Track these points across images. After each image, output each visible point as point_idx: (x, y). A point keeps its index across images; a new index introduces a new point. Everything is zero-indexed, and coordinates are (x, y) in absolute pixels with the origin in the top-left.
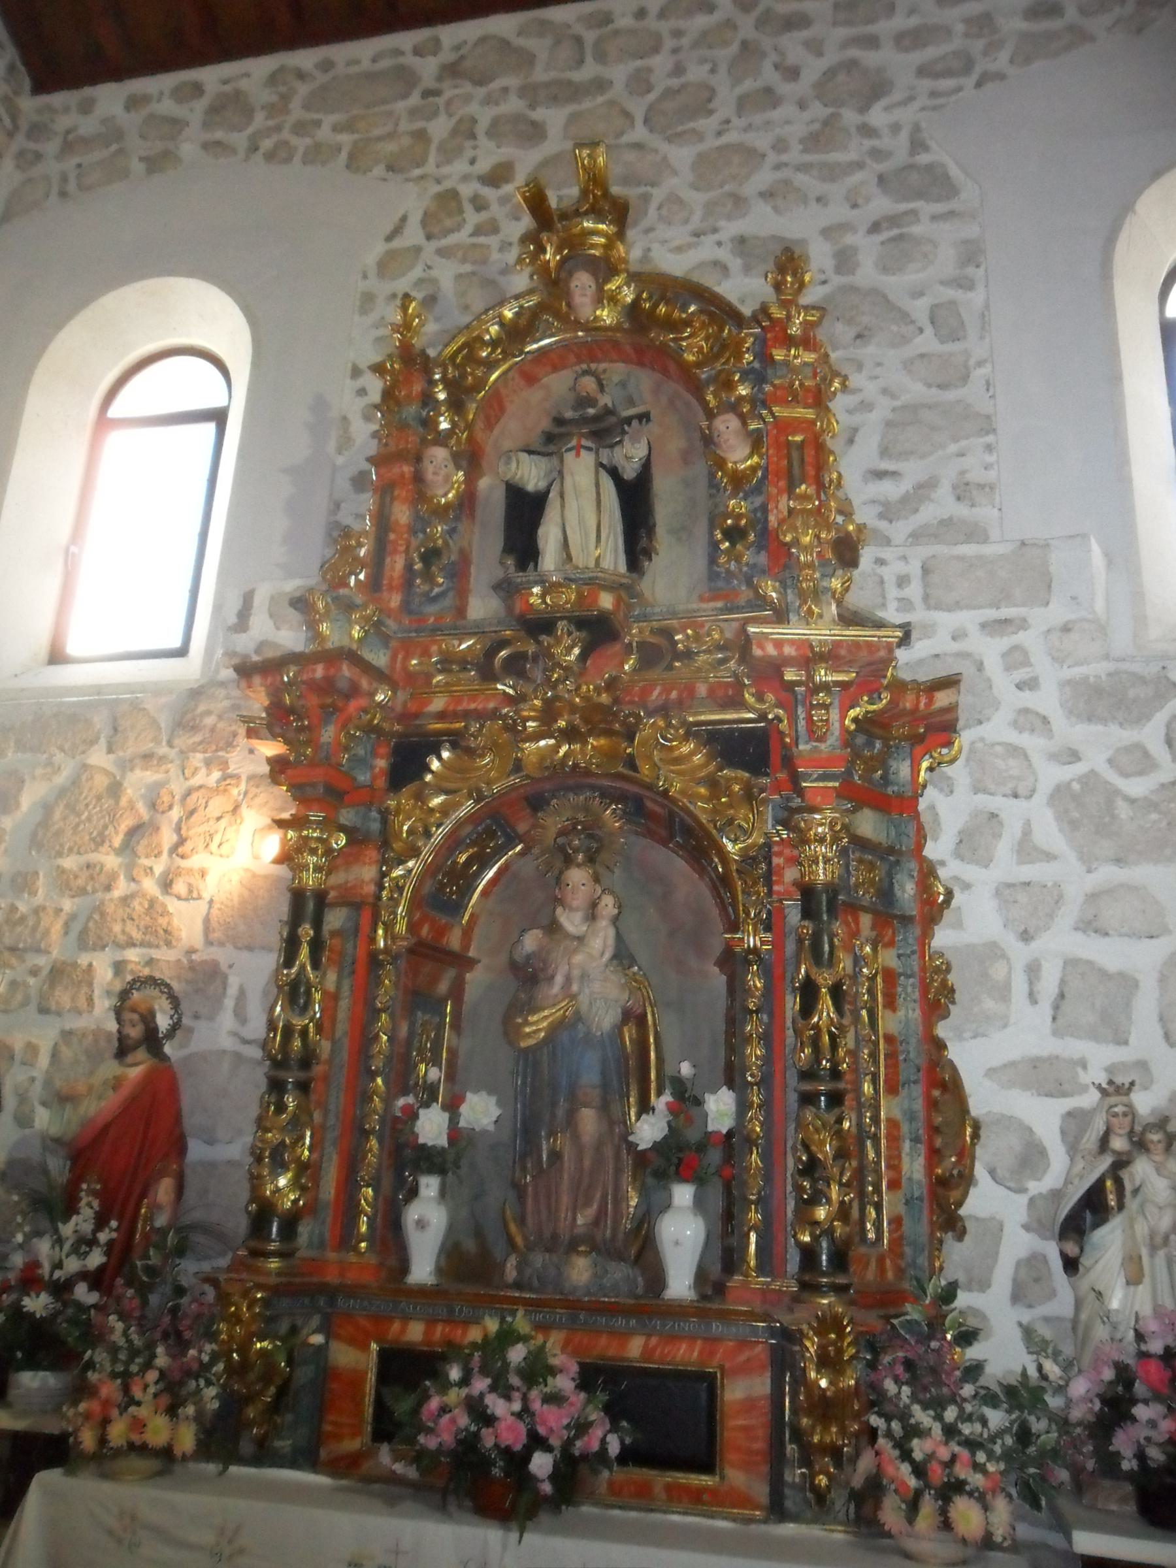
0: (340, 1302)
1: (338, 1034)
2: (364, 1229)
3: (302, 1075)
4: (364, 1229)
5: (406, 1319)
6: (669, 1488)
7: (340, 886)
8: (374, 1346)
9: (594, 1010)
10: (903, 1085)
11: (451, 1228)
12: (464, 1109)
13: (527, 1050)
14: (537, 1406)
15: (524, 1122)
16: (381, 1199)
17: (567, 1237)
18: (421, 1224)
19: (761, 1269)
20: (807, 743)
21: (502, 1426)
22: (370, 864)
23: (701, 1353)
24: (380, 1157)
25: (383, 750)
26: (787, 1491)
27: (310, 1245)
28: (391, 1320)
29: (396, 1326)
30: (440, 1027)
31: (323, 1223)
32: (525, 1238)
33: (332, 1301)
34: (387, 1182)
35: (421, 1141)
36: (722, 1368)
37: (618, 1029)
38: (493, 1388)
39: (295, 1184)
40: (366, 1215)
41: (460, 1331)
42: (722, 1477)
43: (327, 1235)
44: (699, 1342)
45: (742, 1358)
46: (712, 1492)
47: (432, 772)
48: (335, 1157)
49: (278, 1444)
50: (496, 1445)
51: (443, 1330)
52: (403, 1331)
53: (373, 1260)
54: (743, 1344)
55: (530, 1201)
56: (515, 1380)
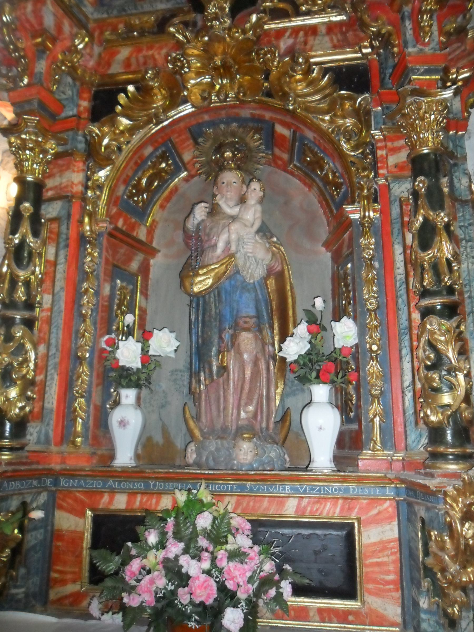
0: (63, 481)
1: (57, 288)
2: (79, 428)
3: (27, 314)
4: (79, 428)
5: (113, 492)
6: (320, 611)
7: (56, 187)
8: (89, 513)
9: (248, 264)
10: (469, 315)
11: (144, 427)
12: (152, 342)
13: (197, 296)
14: (223, 563)
15: (198, 348)
16: (92, 406)
17: (234, 427)
18: (123, 423)
19: (384, 446)
20: (414, 46)
21: (194, 584)
22: (78, 172)
23: (342, 509)
24: (91, 376)
25: (85, 95)
26: (423, 616)
27: (38, 442)
28: (102, 494)
29: (106, 498)
30: (133, 293)
31: (48, 425)
32: (201, 430)
33: (56, 483)
34: (96, 398)
35: (121, 364)
36: (359, 520)
37: (266, 278)
38: (186, 551)
39: (22, 395)
40: (81, 418)
41: (154, 501)
42: (363, 602)
43: (51, 434)
44: (340, 501)
45: (375, 512)
46: (356, 613)
47: (121, 105)
48: (56, 377)
49: (14, 591)
50: (191, 602)
51: (142, 499)
52: (111, 501)
53: (86, 450)
54: (374, 501)
55: (203, 404)
56: (203, 542)
